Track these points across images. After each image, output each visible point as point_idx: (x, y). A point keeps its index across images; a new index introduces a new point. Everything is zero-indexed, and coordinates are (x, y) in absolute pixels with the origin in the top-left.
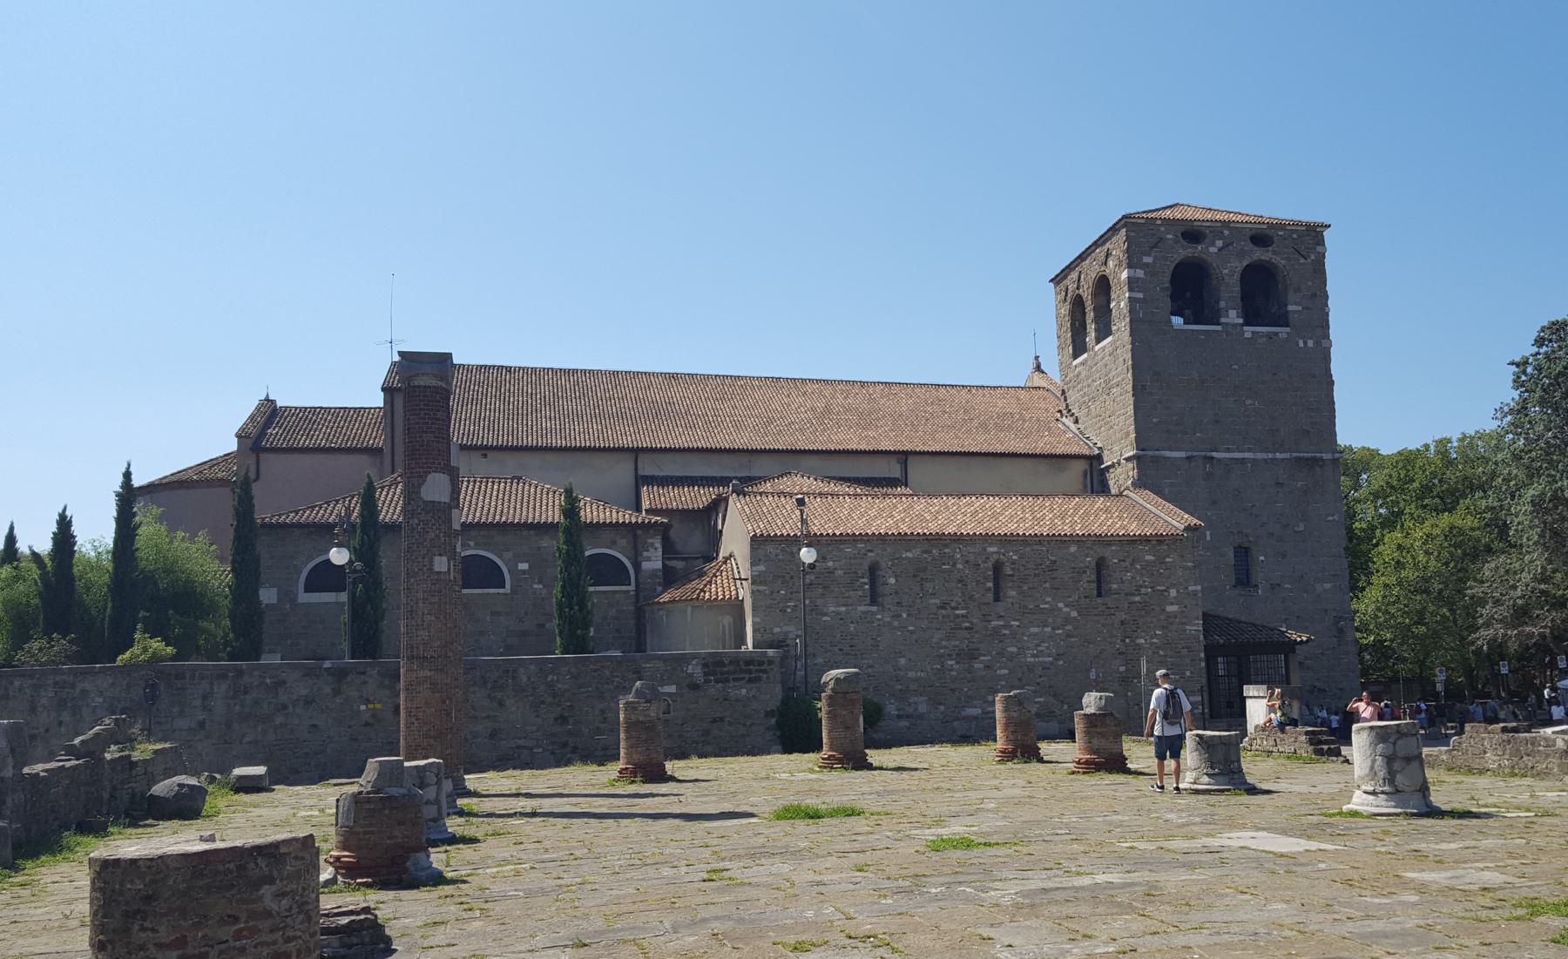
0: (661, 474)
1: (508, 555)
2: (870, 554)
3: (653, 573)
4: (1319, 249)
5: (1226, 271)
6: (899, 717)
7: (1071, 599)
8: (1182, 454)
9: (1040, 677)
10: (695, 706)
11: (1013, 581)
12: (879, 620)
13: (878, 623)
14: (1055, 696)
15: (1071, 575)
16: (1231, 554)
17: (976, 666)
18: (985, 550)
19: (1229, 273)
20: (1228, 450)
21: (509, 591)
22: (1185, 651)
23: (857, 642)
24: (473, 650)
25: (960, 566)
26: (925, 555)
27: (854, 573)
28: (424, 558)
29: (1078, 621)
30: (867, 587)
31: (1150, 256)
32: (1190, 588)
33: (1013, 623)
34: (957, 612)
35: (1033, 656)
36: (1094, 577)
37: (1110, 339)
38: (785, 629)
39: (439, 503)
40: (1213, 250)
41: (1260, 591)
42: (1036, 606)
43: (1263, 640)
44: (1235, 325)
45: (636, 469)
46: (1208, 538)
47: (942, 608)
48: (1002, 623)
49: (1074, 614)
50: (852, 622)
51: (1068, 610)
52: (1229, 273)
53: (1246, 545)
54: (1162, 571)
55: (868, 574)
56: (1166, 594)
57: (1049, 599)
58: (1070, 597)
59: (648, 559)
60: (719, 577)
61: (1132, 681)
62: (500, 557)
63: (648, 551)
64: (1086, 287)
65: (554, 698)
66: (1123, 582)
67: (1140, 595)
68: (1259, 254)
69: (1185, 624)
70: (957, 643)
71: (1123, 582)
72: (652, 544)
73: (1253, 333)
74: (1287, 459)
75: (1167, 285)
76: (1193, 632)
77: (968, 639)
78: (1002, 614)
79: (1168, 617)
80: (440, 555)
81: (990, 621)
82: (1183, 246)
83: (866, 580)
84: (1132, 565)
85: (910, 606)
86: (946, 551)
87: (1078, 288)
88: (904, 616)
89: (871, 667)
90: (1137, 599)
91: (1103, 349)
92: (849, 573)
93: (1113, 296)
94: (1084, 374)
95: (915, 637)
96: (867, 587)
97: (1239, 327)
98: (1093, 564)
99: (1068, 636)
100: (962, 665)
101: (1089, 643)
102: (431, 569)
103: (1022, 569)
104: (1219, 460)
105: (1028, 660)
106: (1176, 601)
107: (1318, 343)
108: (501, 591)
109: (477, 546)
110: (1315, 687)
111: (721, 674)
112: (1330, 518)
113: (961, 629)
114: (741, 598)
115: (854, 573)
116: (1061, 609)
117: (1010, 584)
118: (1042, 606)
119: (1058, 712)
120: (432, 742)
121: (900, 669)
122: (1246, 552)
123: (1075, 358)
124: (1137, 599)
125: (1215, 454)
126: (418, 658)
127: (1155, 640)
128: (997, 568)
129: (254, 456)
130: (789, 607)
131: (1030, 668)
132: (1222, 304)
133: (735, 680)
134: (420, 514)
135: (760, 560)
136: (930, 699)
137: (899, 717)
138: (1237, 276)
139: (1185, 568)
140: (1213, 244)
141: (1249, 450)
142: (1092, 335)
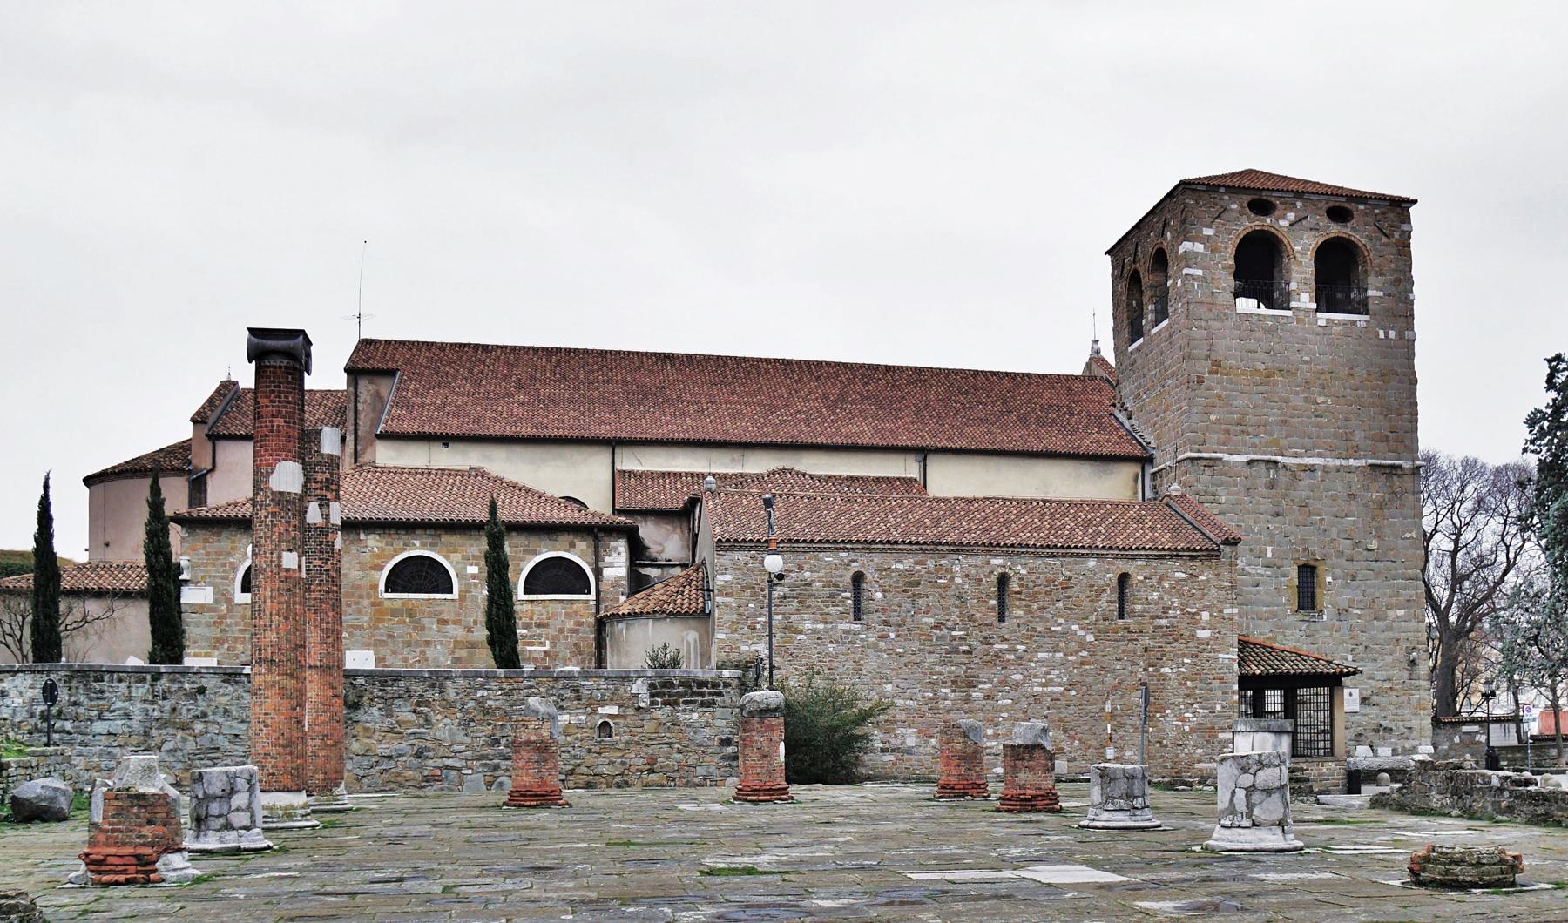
0: (641, 469)
1: (457, 557)
2: (853, 564)
3: (616, 583)
4: (1405, 227)
6: (883, 750)
7: (1087, 622)
8: (1244, 458)
9: (1049, 708)
10: (640, 730)
11: (1020, 599)
12: (862, 640)
13: (861, 644)
14: (1065, 731)
15: (1088, 593)
16: (1295, 574)
17: (974, 695)
18: (988, 563)
20: (1296, 456)
21: (457, 597)
22: (1216, 683)
23: (836, 664)
24: (419, 661)
25: (958, 580)
26: (918, 567)
27: (835, 585)
28: (272, 553)
29: (1094, 646)
30: (849, 602)
31: (1211, 227)
32: (1227, 611)
33: (1018, 647)
34: (954, 633)
35: (1042, 685)
36: (1115, 597)
37: (1166, 322)
38: (754, 648)
39: (289, 493)
40: (1284, 223)
41: (1325, 617)
42: (1046, 629)
43: (1305, 671)
44: (1307, 311)
45: (613, 463)
46: (1269, 555)
48: (1006, 647)
49: (1090, 638)
50: (831, 642)
51: (1082, 633)
53: (1312, 563)
54: (1194, 591)
55: (851, 587)
56: (1197, 617)
57: (1061, 620)
58: (1087, 618)
59: (611, 566)
60: (687, 587)
61: (1154, 716)
62: (447, 558)
63: (610, 556)
64: (1143, 260)
65: (484, 715)
66: (1149, 604)
67: (1167, 618)
68: (1335, 230)
69: (1219, 652)
70: (953, 668)
71: (1149, 604)
72: (615, 549)
74: (1362, 467)
75: (1232, 262)
76: (1227, 661)
78: (1006, 636)
79: (1199, 644)
80: (290, 550)
83: (849, 594)
84: (1159, 582)
85: (899, 626)
86: (943, 562)
87: (1134, 262)
88: (892, 635)
90: (1164, 622)
91: (1159, 333)
92: (829, 586)
93: (1171, 273)
94: (1139, 362)
95: (904, 660)
96: (849, 602)
98: (1115, 581)
99: (1082, 663)
100: (957, 694)
102: (279, 566)
103: (1031, 585)
105: (1035, 689)
106: (1210, 626)
107: (1400, 335)
108: (448, 596)
109: (423, 546)
110: (1381, 725)
111: (670, 696)
112: (1408, 535)
113: (958, 653)
114: (707, 612)
115: (835, 585)
117: (1017, 603)
118: (1053, 628)
119: (1067, 749)
122: (1313, 573)
123: (1133, 342)
124: (1164, 622)
125: (1279, 458)
126: (266, 660)
127: (1183, 670)
128: (1003, 580)
129: (210, 445)
130: (758, 623)
131: (1037, 699)
132: (1293, 286)
133: (685, 703)
134: (269, 505)
135: (726, 569)
136: (920, 732)
137: (883, 750)
138: (1310, 255)
139: (1221, 588)
140: (1284, 217)
141: (1320, 455)
142: (1151, 317)
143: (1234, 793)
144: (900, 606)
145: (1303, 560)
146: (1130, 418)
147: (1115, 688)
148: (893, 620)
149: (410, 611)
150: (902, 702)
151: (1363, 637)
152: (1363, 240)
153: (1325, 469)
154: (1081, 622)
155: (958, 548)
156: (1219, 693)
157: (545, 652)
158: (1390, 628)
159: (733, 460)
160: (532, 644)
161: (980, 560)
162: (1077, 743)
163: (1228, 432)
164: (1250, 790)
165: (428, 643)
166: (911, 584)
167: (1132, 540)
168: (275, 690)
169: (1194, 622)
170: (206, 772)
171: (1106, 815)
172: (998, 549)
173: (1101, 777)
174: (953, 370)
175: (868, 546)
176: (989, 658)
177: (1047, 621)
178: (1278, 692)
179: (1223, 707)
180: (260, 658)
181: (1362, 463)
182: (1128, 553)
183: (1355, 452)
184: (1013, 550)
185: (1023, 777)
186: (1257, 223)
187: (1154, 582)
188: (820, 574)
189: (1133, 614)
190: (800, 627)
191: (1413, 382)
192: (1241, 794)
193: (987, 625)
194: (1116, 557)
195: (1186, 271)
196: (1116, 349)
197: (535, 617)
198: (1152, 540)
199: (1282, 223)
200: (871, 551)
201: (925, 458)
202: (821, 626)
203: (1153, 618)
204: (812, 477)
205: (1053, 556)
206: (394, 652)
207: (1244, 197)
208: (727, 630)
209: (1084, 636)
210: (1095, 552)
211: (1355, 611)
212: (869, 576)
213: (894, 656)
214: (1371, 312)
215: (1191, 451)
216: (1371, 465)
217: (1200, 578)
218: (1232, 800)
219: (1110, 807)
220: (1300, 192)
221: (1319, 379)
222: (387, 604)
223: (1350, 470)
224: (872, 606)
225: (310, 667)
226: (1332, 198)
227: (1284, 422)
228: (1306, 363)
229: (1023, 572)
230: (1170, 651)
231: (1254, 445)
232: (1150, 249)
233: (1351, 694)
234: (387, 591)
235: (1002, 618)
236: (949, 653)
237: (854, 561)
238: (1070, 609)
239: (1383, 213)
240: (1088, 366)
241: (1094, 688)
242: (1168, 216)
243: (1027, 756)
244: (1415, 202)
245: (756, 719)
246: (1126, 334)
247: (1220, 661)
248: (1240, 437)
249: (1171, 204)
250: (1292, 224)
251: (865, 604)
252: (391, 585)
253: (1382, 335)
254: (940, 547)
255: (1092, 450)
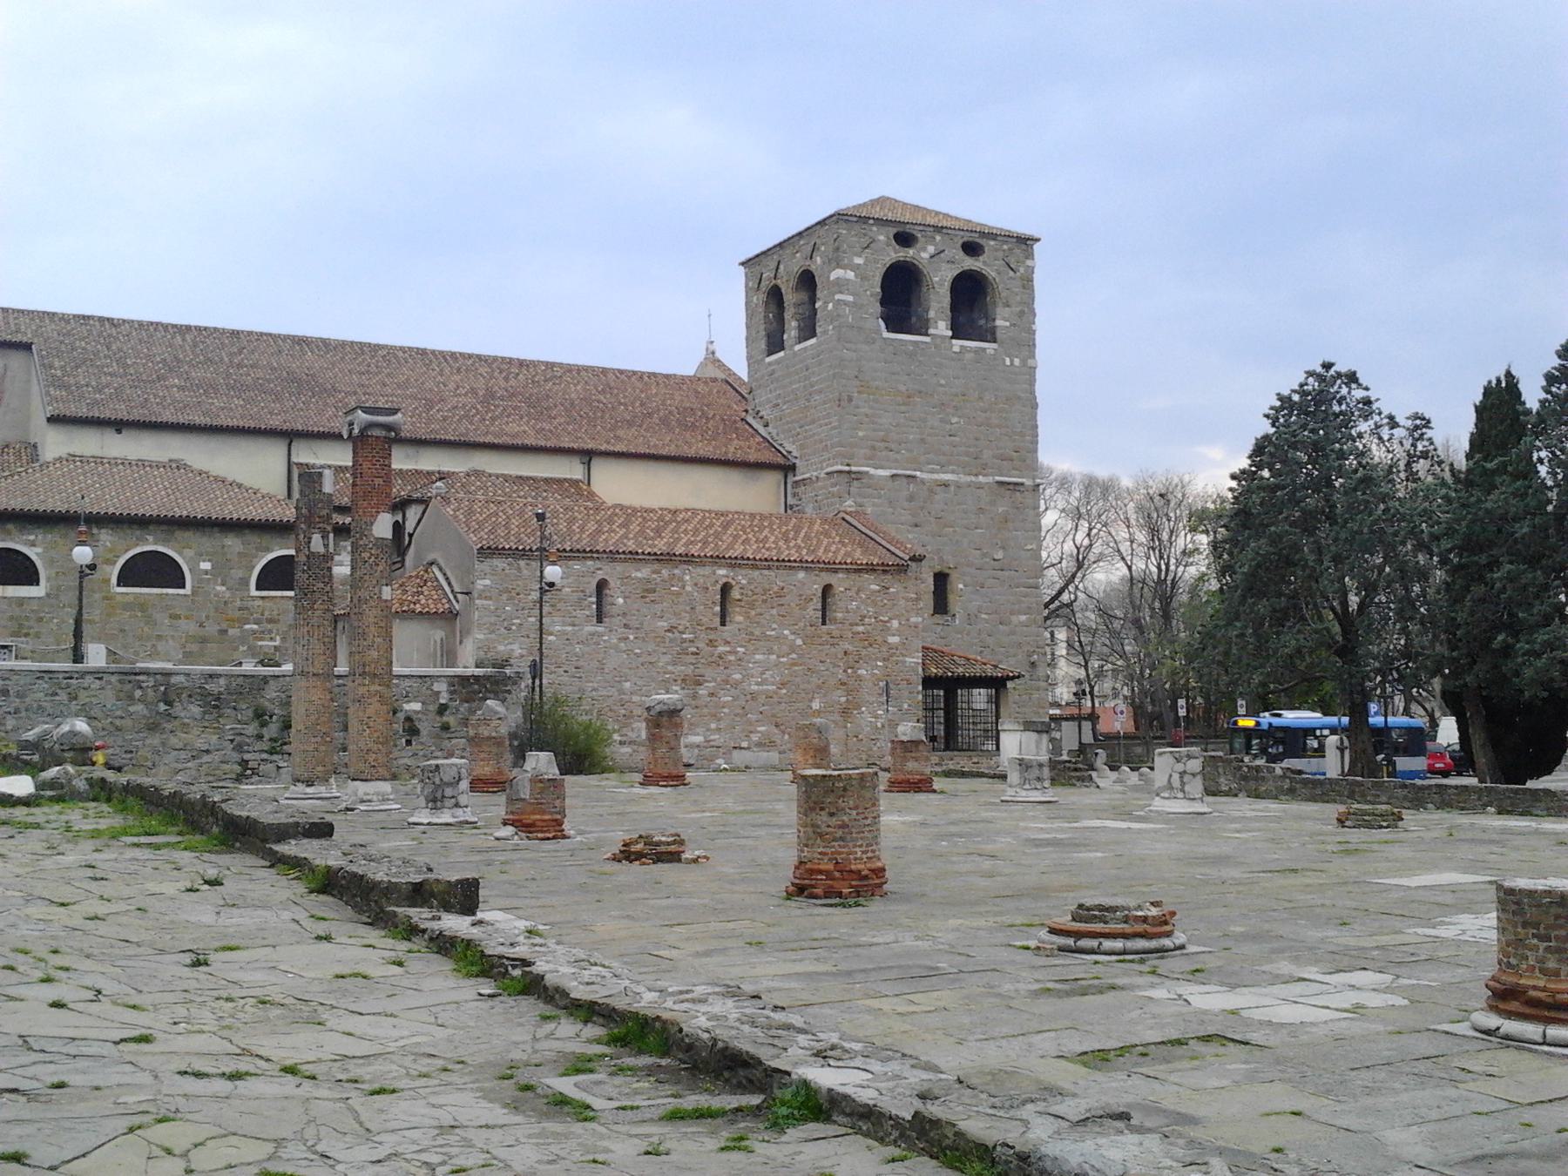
1: (189, 553)
2: (599, 572)
4: (1029, 263)
5: (937, 279)
12: (605, 641)
15: (799, 602)
16: (931, 580)
17: (701, 692)
19: (940, 280)
20: (932, 471)
21: (189, 593)
25: (688, 588)
26: (654, 576)
27: (582, 591)
32: (913, 620)
33: (739, 649)
34: (684, 636)
35: (758, 684)
36: (819, 606)
41: (957, 622)
45: (289, 455)
47: (669, 631)
48: (728, 649)
49: (799, 642)
51: (793, 637)
52: (940, 280)
53: (947, 571)
55: (595, 595)
56: (888, 625)
57: (774, 626)
62: (180, 554)
66: (848, 612)
68: (969, 263)
71: (848, 612)
73: (961, 346)
75: (879, 290)
77: (693, 664)
78: (729, 639)
80: (387, 585)
81: (716, 647)
82: (894, 248)
85: (637, 629)
88: (631, 637)
89: (594, 689)
90: (861, 629)
92: (577, 591)
97: (947, 340)
98: (820, 591)
99: (795, 664)
100: (686, 691)
101: (813, 672)
102: (380, 598)
103: (750, 593)
104: (923, 482)
106: (898, 633)
107: (1024, 362)
108: (181, 591)
112: (1029, 547)
115: (582, 591)
116: (786, 637)
117: (738, 609)
118: (768, 633)
119: (779, 742)
120: (380, 746)
121: (624, 694)
124: (861, 629)
125: (918, 474)
128: (726, 589)
130: (513, 624)
131: (754, 696)
132: (932, 314)
137: (621, 743)
138: (947, 285)
139: (907, 600)
140: (924, 249)
141: (953, 472)
142: (794, 333)
143: (1171, 776)
144: (638, 611)
145: (938, 568)
146: (766, 425)
147: (819, 687)
148: (631, 624)
149: (142, 605)
150: (639, 698)
151: (990, 641)
152: (993, 274)
153: (958, 486)
154: (791, 628)
155: (688, 559)
156: (906, 693)
157: (275, 647)
158: (1013, 633)
159: (408, 456)
160: (262, 639)
161: (707, 570)
162: (786, 737)
163: (873, 448)
164: (1182, 774)
165: (159, 637)
166: (648, 590)
167: (831, 554)
168: (377, 698)
169: (886, 630)
170: (442, 765)
171: (1024, 793)
172: (723, 560)
173: (1020, 765)
174: (583, 367)
175: (613, 556)
176: (713, 659)
177: (763, 626)
178: (959, 691)
179: (909, 706)
180: (364, 672)
181: (990, 479)
182: (831, 567)
183: (983, 469)
184: (735, 563)
185: (911, 765)
186: (901, 254)
187: (852, 593)
188: (570, 581)
189: (835, 621)
190: (551, 629)
191: (1035, 406)
192: (1176, 777)
193: (711, 629)
194: (821, 570)
195: (838, 297)
196: (749, 358)
197: (266, 613)
198: (847, 554)
199: (922, 254)
200: (614, 560)
201: (590, 460)
202: (570, 628)
203: (851, 625)
204: (490, 475)
205: (769, 568)
206: (125, 647)
207: (890, 229)
208: (486, 631)
209: (794, 640)
210: (805, 565)
211: (983, 616)
212: (614, 583)
213: (632, 656)
214: (998, 340)
215: (842, 465)
216: (997, 482)
217: (892, 590)
218: (1169, 781)
219: (1027, 786)
220: (940, 228)
221: (952, 400)
222: (119, 598)
223: (980, 487)
224: (614, 610)
225: (314, 675)
226: (968, 234)
227: (922, 440)
228: (942, 385)
229: (744, 582)
230: (866, 655)
231: (896, 461)
232: (796, 270)
233: (980, 694)
234: (118, 585)
235: (723, 623)
236: (680, 654)
237: (600, 569)
238: (783, 616)
239: (1010, 249)
240: (702, 365)
241: (801, 687)
242: (818, 242)
243: (914, 749)
244: (1038, 240)
245: (665, 719)
246: (763, 345)
247: (907, 664)
248: (884, 453)
249: (822, 231)
250: (932, 257)
251: (607, 608)
252: (123, 580)
253: (1008, 362)
254: (673, 558)
255: (739, 456)
